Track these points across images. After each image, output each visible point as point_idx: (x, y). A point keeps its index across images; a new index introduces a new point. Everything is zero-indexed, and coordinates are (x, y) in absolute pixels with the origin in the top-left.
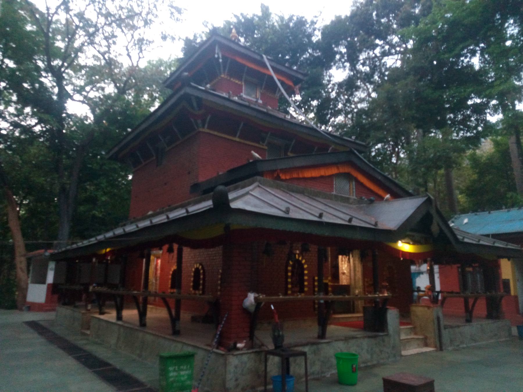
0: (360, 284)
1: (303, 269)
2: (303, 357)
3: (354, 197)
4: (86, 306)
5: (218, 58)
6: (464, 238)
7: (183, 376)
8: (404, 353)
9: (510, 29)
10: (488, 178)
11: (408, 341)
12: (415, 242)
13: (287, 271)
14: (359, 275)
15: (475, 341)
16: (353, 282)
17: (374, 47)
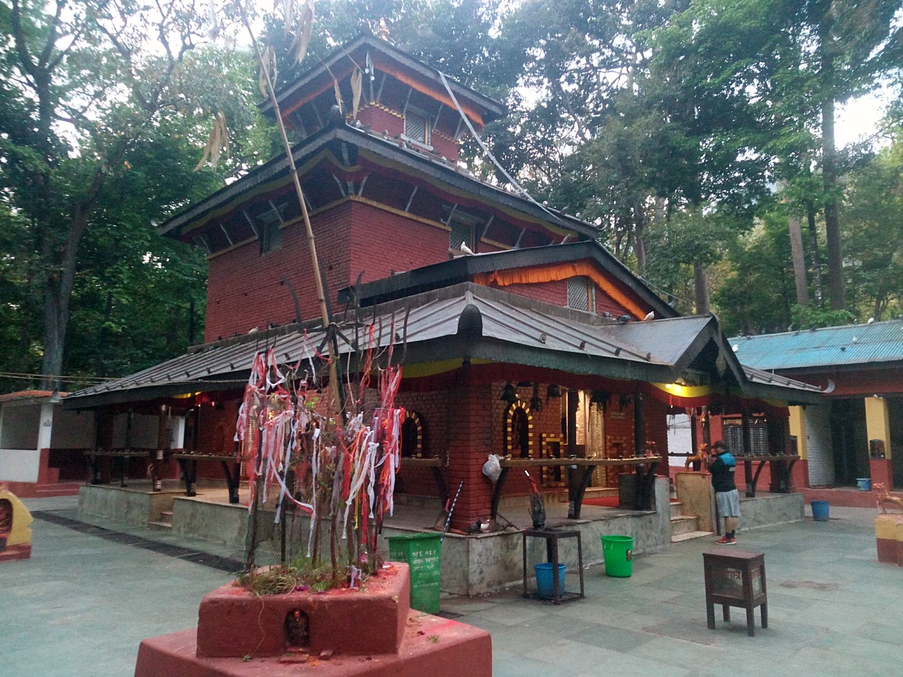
0: (600, 443)
1: (527, 423)
2: (576, 538)
3: (594, 314)
4: (154, 484)
5: (370, 73)
6: (752, 377)
7: (429, 564)
8: (674, 539)
9: (805, 44)
10: (753, 277)
11: (676, 523)
12: (689, 383)
13: (505, 426)
14: (599, 430)
15: (760, 523)
16: (589, 441)
17: (588, 53)
